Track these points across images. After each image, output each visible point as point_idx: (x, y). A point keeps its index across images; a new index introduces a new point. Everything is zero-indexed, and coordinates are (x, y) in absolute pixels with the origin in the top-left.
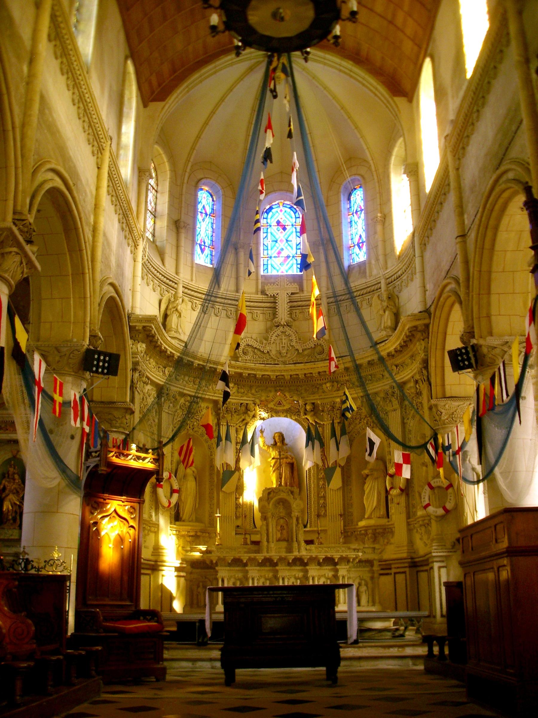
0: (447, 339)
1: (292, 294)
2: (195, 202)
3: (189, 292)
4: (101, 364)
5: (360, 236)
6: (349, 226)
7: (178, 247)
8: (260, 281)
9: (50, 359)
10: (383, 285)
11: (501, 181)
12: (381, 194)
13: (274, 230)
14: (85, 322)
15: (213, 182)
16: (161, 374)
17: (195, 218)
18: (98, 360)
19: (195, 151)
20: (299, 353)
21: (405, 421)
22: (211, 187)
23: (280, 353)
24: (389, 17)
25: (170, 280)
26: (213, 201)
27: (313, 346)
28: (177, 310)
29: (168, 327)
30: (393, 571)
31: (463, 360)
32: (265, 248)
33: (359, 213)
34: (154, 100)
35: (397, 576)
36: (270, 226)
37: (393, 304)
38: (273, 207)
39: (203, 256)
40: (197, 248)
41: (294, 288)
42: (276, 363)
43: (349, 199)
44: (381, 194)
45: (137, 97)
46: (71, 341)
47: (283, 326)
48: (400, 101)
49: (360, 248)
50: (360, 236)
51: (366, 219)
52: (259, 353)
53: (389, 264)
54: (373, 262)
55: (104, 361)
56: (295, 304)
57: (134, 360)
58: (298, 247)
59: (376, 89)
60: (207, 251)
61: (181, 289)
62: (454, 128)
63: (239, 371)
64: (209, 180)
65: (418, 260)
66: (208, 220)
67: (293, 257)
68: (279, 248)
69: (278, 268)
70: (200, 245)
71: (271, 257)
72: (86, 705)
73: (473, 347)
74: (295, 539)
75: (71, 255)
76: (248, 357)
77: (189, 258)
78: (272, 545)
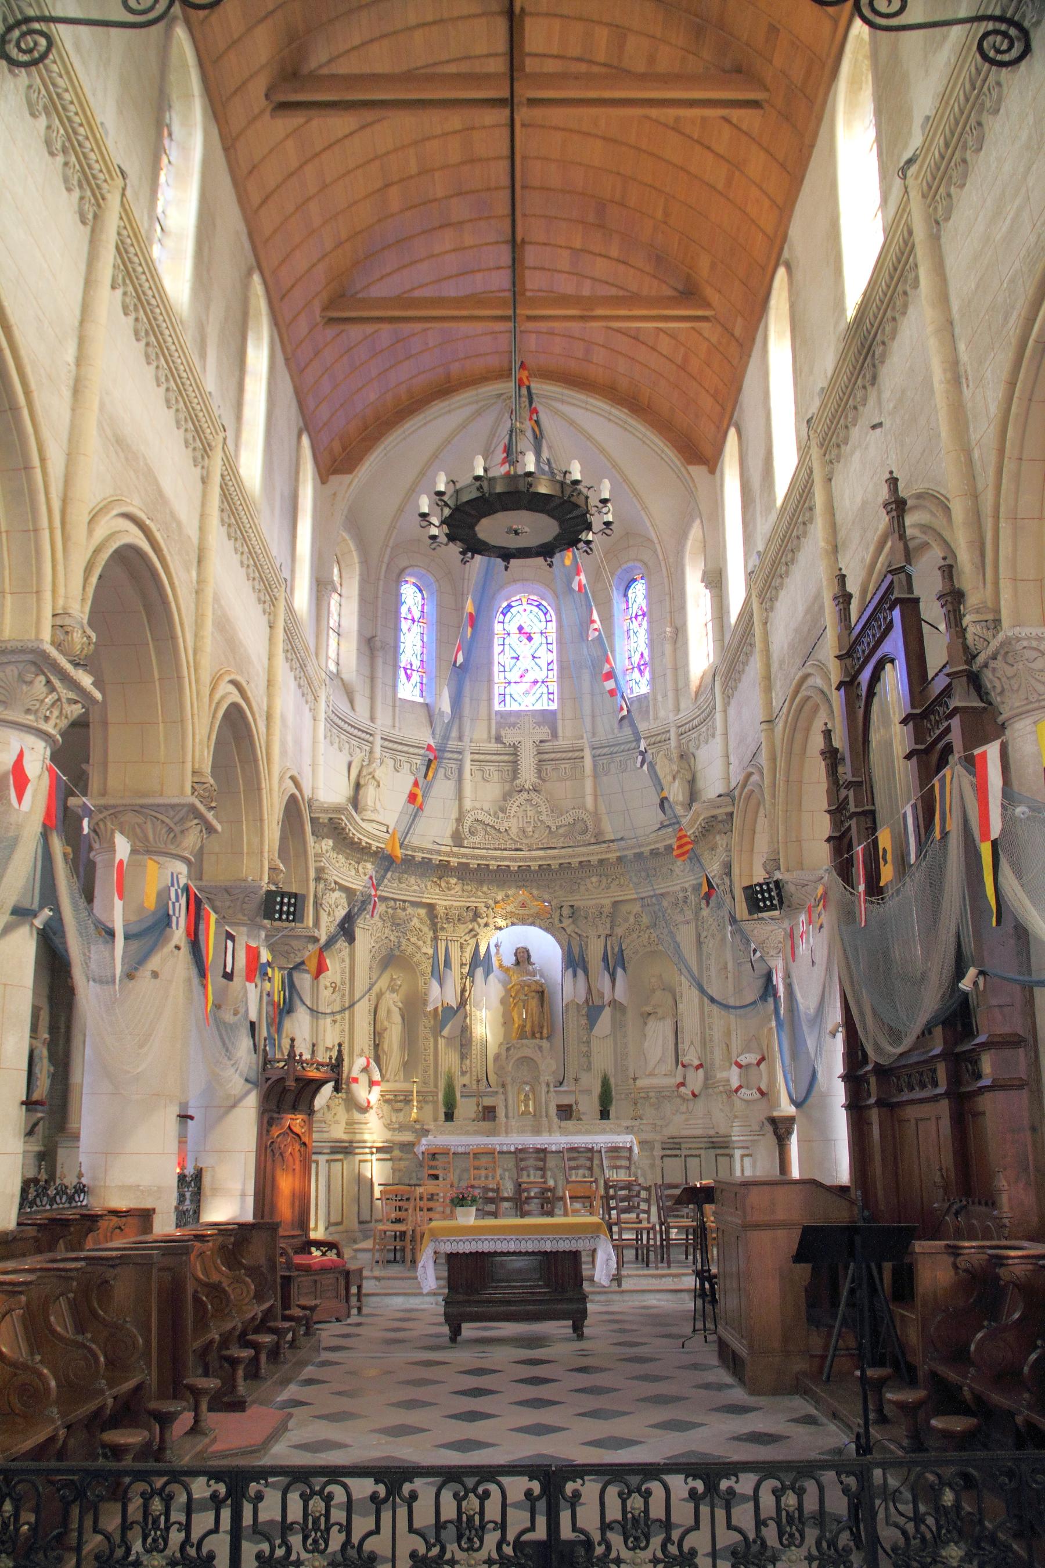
0: (756, 840)
1: (541, 742)
2: (397, 601)
3: (390, 745)
4: (285, 908)
5: (642, 655)
6: (626, 637)
7: (372, 679)
8: (493, 722)
9: (218, 904)
10: (673, 735)
11: (803, 688)
12: (672, 598)
13: (514, 639)
14: (262, 852)
15: (424, 572)
16: (353, 873)
17: (397, 629)
18: (282, 903)
19: (396, 531)
20: (550, 832)
21: (702, 939)
22: (420, 577)
23: (524, 832)
24: (679, 361)
25: (363, 731)
26: (423, 599)
27: (571, 821)
28: (373, 777)
29: (361, 805)
30: (684, 1152)
31: (764, 899)
32: (502, 669)
33: (640, 618)
34: (336, 472)
35: (688, 1159)
36: (509, 634)
37: (687, 767)
38: (513, 604)
39: (409, 686)
40: (402, 672)
41: (544, 733)
42: (518, 846)
43: (626, 595)
44: (672, 598)
45: (314, 479)
46: (245, 880)
47: (528, 791)
48: (698, 472)
49: (641, 672)
50: (642, 655)
51: (650, 631)
52: (493, 831)
53: (683, 706)
54: (659, 698)
55: (289, 904)
56: (546, 756)
57: (318, 864)
58: (550, 667)
59: (663, 451)
60: (415, 677)
61: (378, 742)
62: (762, 562)
63: (464, 860)
64: (416, 569)
65: (719, 716)
66: (416, 629)
67: (543, 682)
68: (523, 669)
69: (519, 700)
70: (405, 669)
71: (509, 683)
72: (310, 1368)
73: (777, 883)
74: (544, 1114)
75: (242, 768)
76: (476, 839)
77: (389, 694)
78: (513, 1122)
